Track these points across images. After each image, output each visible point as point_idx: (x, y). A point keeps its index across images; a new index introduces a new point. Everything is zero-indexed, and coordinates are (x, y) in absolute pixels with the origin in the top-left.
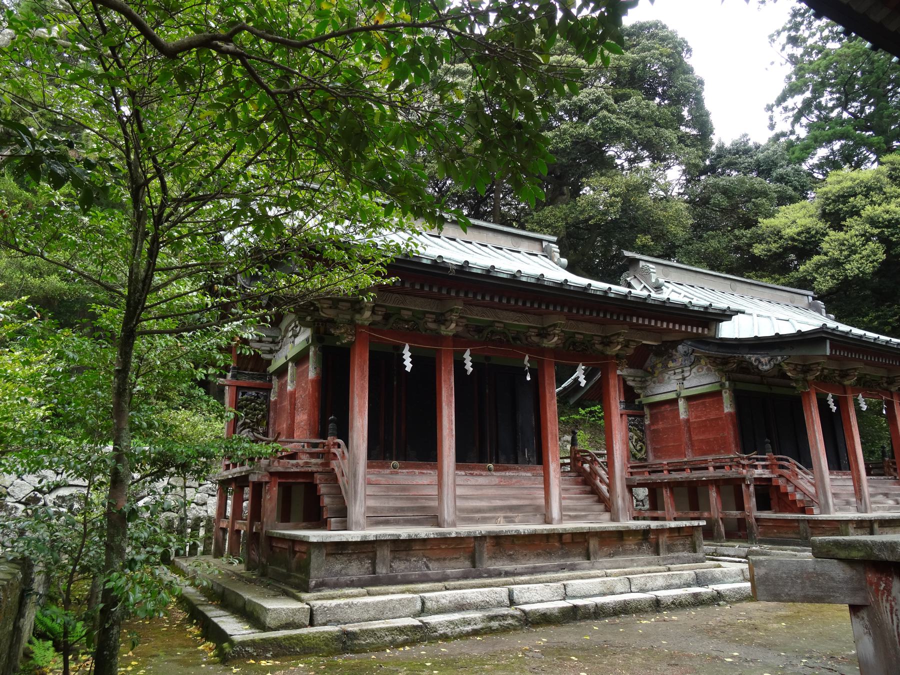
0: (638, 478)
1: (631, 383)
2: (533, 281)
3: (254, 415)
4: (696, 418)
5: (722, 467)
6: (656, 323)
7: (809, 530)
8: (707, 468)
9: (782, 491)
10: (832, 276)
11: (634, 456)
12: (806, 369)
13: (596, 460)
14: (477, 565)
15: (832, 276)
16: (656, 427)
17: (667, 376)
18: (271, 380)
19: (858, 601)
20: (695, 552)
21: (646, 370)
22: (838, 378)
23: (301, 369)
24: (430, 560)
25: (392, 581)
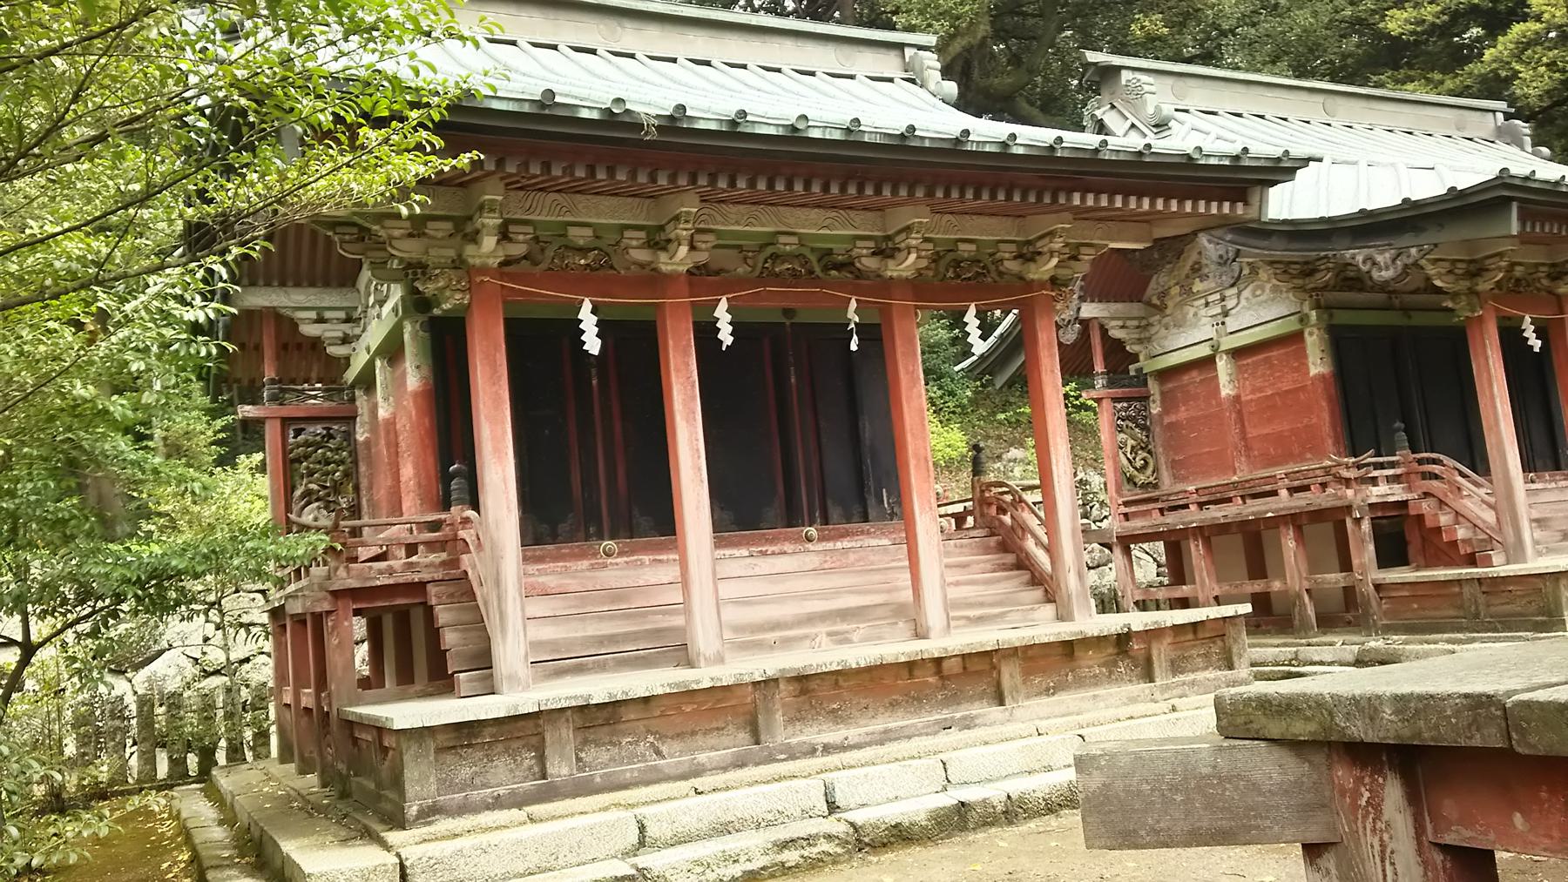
0: (1137, 525)
1: (1116, 333)
2: (837, 135)
3: (327, 474)
4: (1253, 392)
5: (1306, 488)
6: (1126, 203)
7: (1482, 599)
8: (1274, 493)
9: (1429, 523)
10: (1551, 65)
11: (1130, 480)
12: (1476, 270)
13: (1021, 501)
14: (763, 738)
15: (1551, 65)
16: (1173, 418)
17: (1192, 311)
18: (353, 400)
19: (1314, 836)
20: (1231, 667)
21: (1149, 304)
22: (1545, 282)
23: (398, 372)
24: (662, 737)
25: (582, 788)
